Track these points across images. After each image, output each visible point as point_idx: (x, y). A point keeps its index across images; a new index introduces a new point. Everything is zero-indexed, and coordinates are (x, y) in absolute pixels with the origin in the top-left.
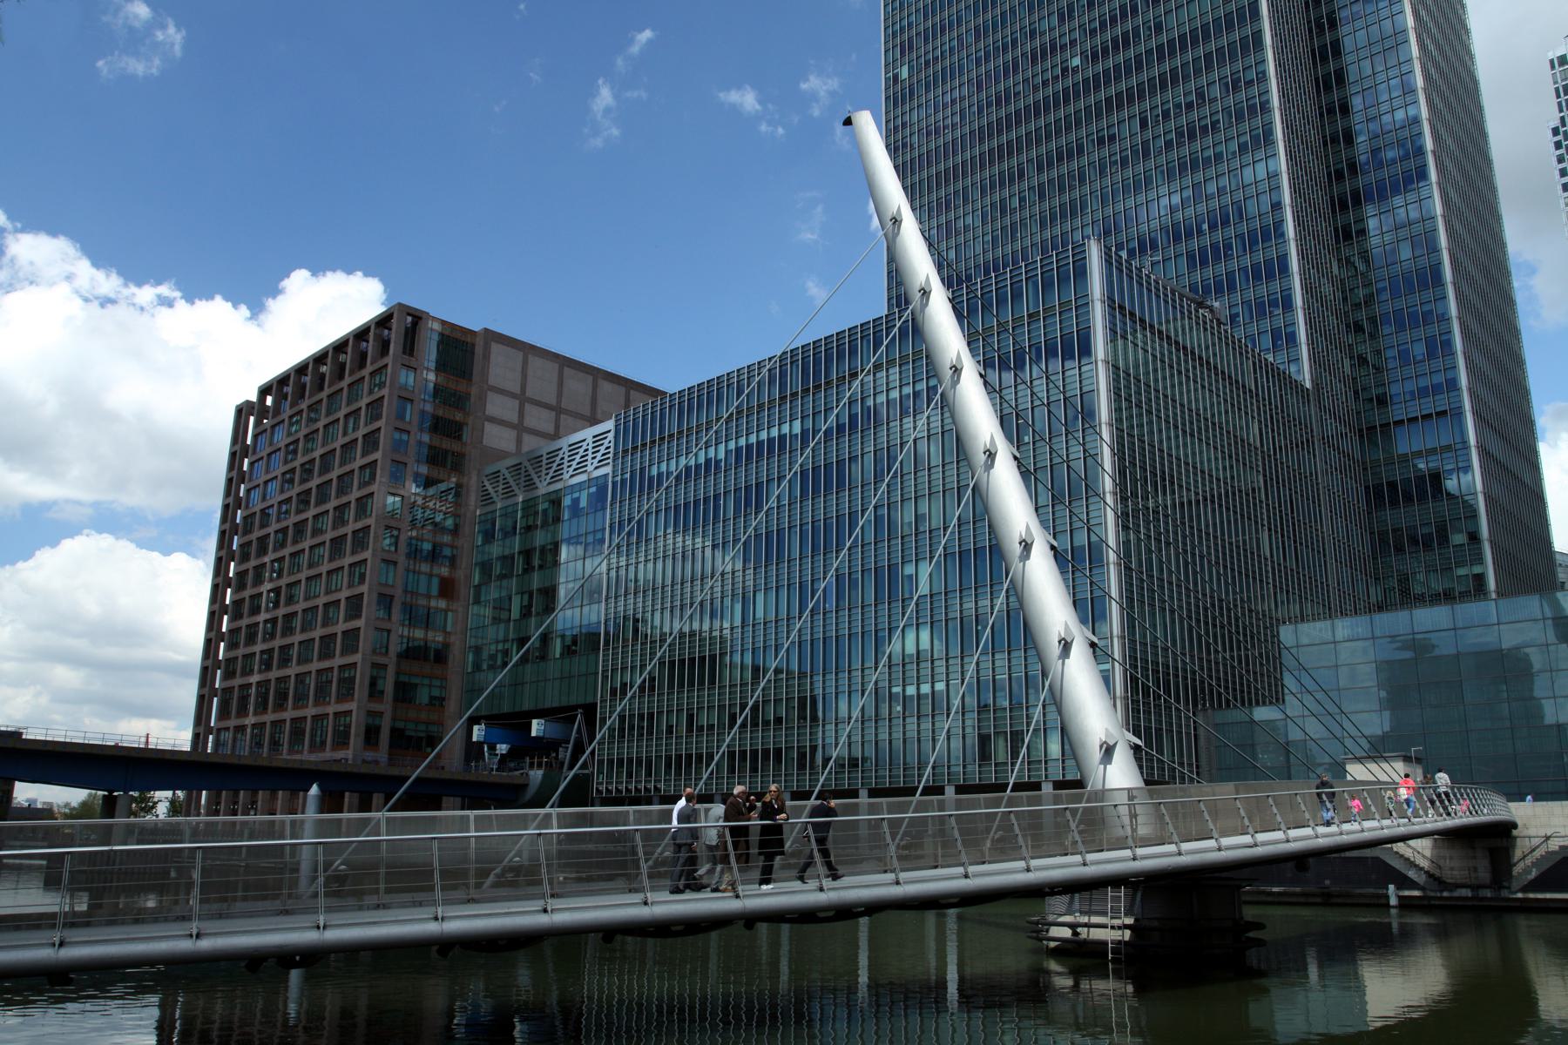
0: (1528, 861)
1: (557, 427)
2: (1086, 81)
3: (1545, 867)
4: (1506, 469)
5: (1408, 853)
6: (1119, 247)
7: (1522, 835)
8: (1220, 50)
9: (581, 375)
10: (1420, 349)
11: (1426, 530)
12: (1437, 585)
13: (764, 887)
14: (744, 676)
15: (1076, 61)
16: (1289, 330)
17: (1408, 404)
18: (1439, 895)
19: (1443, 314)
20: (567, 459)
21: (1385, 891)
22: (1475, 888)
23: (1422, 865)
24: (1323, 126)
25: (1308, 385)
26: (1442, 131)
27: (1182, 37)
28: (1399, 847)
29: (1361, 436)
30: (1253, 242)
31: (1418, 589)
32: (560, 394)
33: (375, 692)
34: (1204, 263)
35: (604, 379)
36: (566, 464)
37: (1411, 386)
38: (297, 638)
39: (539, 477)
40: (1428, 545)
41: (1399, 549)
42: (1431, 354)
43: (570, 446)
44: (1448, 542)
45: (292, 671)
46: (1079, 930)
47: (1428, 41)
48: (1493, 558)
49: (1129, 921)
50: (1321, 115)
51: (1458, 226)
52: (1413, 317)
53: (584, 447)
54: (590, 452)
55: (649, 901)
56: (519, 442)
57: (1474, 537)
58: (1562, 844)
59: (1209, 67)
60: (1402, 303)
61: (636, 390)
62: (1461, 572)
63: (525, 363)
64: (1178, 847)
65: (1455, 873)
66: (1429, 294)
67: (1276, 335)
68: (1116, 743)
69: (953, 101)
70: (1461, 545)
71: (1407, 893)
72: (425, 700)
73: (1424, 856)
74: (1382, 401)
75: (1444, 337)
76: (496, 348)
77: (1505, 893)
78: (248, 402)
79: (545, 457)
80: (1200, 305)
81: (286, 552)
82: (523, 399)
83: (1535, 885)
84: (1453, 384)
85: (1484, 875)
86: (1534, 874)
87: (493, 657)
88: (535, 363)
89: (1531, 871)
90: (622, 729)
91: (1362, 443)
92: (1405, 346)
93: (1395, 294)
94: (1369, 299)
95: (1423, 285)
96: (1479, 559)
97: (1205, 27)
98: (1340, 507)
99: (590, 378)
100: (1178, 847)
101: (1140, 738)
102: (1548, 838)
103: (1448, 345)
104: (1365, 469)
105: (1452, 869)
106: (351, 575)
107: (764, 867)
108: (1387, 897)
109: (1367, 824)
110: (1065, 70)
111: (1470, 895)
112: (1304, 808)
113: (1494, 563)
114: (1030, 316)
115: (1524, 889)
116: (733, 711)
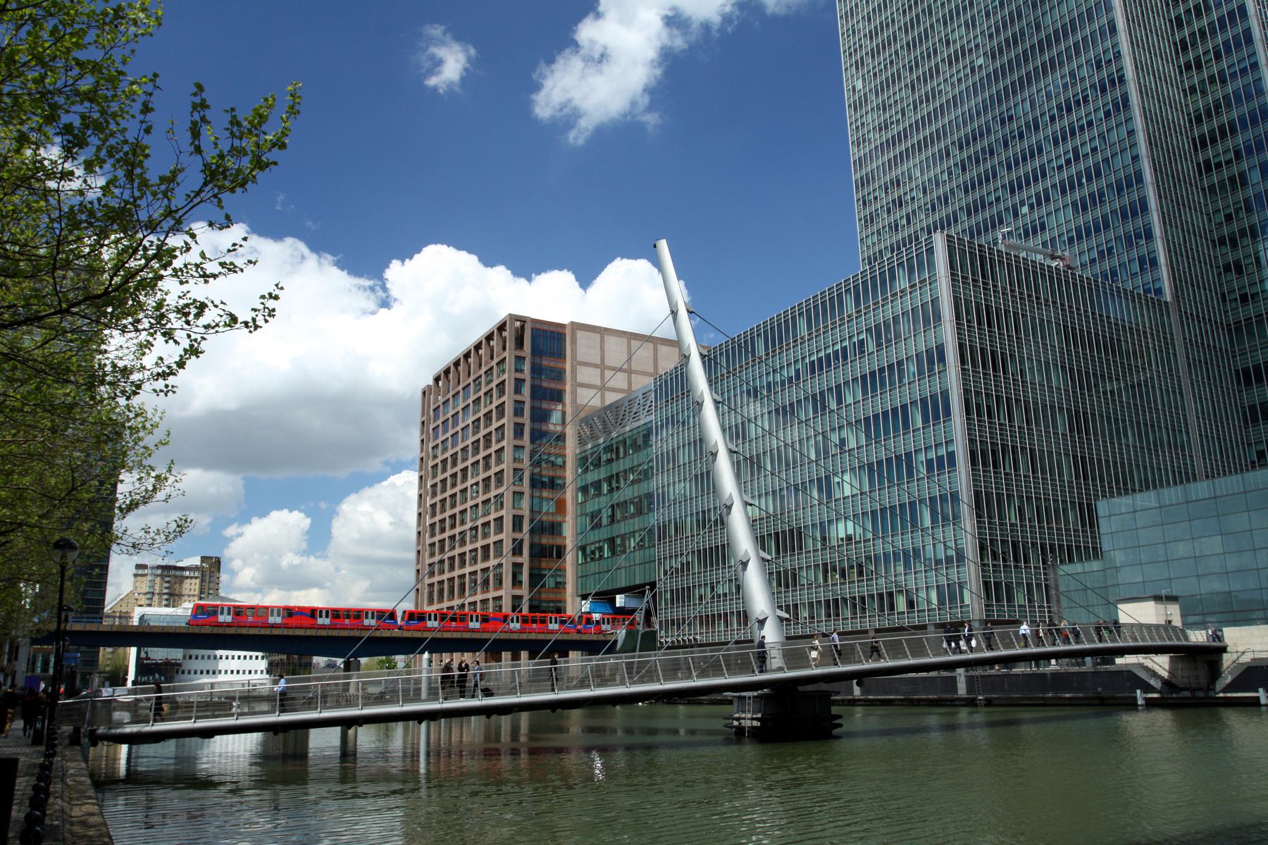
2: (988, 75)
6: (1022, 203)
8: (1084, 39)
14: (945, 510)
15: (981, 61)
22: (1193, 690)
27: (1056, 32)
30: (1120, 190)
33: (516, 582)
38: (468, 547)
45: (468, 569)
56: (603, 398)
59: (1077, 53)
63: (602, 341)
67: (1142, 261)
68: (766, 619)
69: (896, 102)
71: (1150, 695)
72: (552, 585)
76: (580, 334)
77: (1211, 694)
78: (429, 386)
81: (457, 489)
82: (602, 367)
85: (1203, 681)
87: (593, 552)
88: (611, 341)
97: (1072, 21)
101: (789, 613)
106: (496, 503)
108: (1135, 698)
110: (973, 70)
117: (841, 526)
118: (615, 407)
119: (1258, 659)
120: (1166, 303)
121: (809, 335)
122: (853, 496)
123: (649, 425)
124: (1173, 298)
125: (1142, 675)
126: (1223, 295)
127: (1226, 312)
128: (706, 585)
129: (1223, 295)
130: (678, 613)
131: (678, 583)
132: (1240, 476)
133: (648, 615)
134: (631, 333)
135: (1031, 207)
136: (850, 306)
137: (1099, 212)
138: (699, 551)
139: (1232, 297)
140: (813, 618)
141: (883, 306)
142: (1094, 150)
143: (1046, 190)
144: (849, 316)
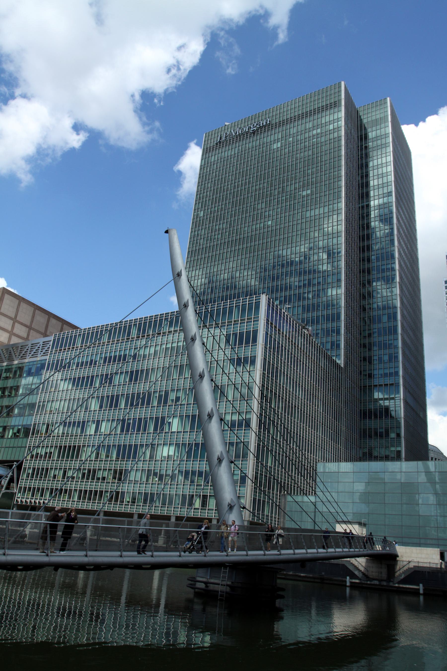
0: (401, 571)
1: (28, 335)
3: (407, 574)
4: (414, 410)
5: (356, 564)
6: (276, 299)
7: (400, 560)
9: (43, 314)
10: (386, 358)
11: (381, 430)
12: (383, 452)
13: (62, 553)
16: (338, 343)
17: (380, 379)
18: (366, 582)
19: (396, 346)
20: (29, 350)
21: (345, 579)
22: (380, 581)
23: (361, 569)
24: (360, 265)
25: (342, 366)
26: (403, 275)
28: (353, 560)
29: (361, 389)
31: (375, 453)
32: (32, 321)
34: (308, 311)
35: (53, 318)
36: (29, 352)
37: (381, 372)
39: (15, 356)
40: (381, 436)
41: (370, 437)
42: (390, 360)
43: (32, 344)
44: (388, 436)
46: (208, 585)
47: (401, 241)
48: (405, 445)
49: (229, 583)
50: (360, 261)
51: (405, 312)
52: (385, 345)
53: (38, 346)
54: (40, 349)
55: (6, 554)
57: (399, 435)
58: (415, 565)
60: (381, 339)
61: (66, 325)
62: (393, 449)
64: (294, 551)
65: (373, 574)
66: (392, 337)
67: (332, 344)
68: (235, 505)
70: (393, 438)
71: (354, 581)
73: (362, 566)
74: (370, 376)
75: (396, 355)
76: (7, 296)
77: (391, 584)
79: (20, 347)
80: (304, 328)
83: (403, 581)
84: (397, 374)
86: (403, 576)
89: (402, 575)
90: (33, 474)
91: (361, 392)
92: (381, 356)
93: (379, 335)
94: (370, 335)
95: (390, 333)
96: (400, 445)
98: (349, 417)
99: (47, 317)
100: (294, 551)
102: (409, 562)
103: (397, 357)
104: (361, 403)
105: (372, 572)
107: (63, 543)
108: (346, 582)
109: (338, 550)
111: (378, 583)
112: (303, 541)
113: (405, 447)
114: (235, 321)
115: (399, 583)
116: (28, 472)
117: (166, 449)
118: (15, 346)
119: (421, 567)
120: (342, 367)
121: (108, 342)
122: (177, 432)
123: (43, 362)
124: (344, 366)
125: (351, 568)
126: (361, 372)
127: (361, 380)
128: (60, 469)
129: (361, 372)
130: (35, 483)
131: (41, 464)
132: (433, 462)
133: (11, 480)
134: (37, 306)
135: (281, 302)
136: (105, 339)
137: (315, 314)
138: (61, 447)
139: (365, 373)
140: (135, 502)
141: (157, 337)
142: (319, 283)
143: (290, 296)
144: (132, 338)
